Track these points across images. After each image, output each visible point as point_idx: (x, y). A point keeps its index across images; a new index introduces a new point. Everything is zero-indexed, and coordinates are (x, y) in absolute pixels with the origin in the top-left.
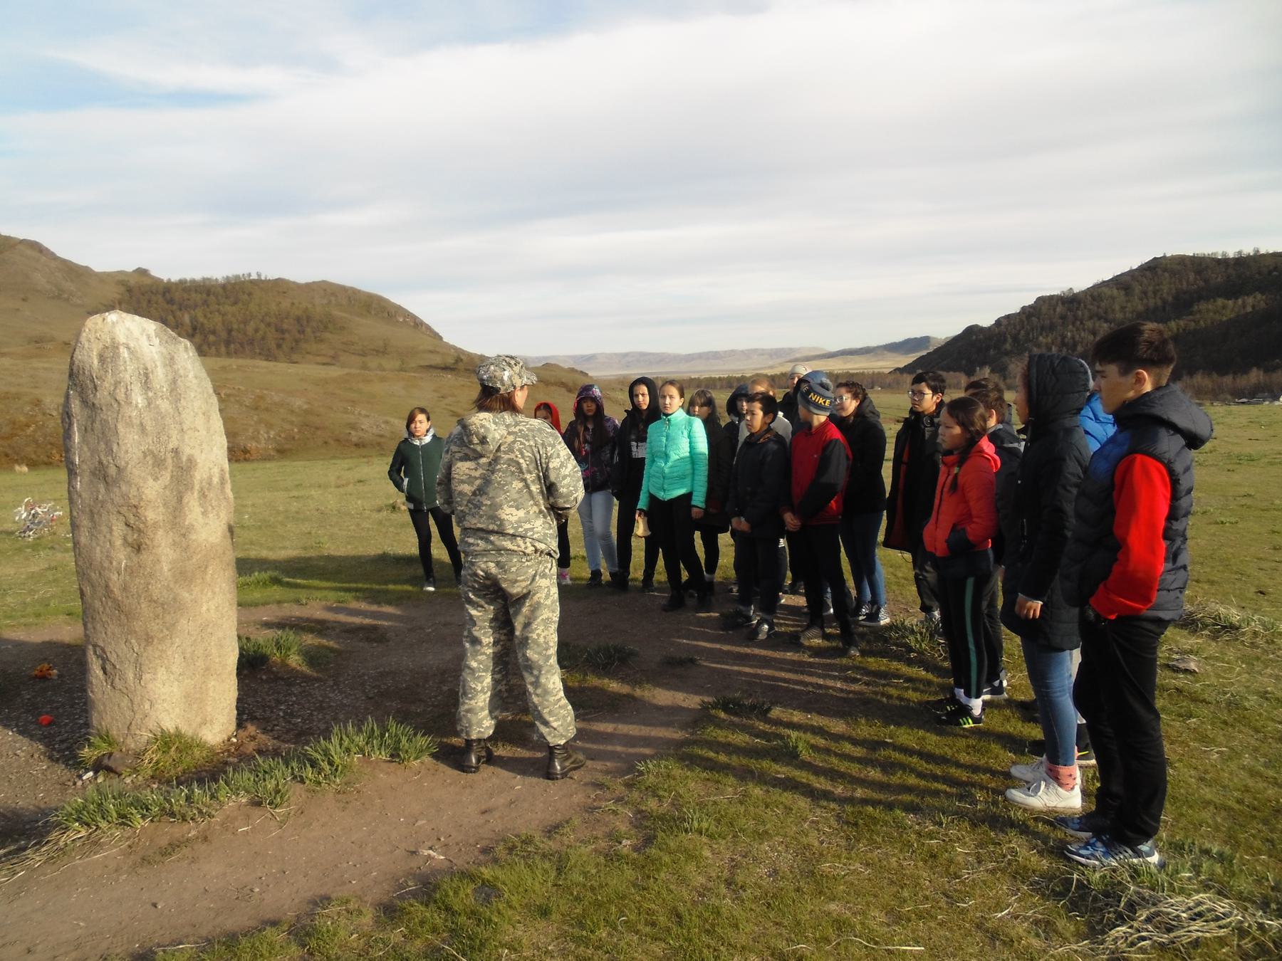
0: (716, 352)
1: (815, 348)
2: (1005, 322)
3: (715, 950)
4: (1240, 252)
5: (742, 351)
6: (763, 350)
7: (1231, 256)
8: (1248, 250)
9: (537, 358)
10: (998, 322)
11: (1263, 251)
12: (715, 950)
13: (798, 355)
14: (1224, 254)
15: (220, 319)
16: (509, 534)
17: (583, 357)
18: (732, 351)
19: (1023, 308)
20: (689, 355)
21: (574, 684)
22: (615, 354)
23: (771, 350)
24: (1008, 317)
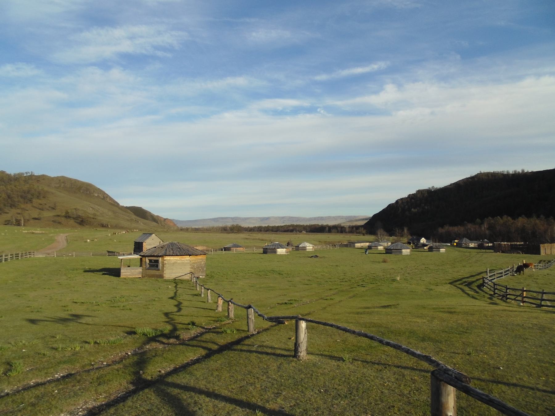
0: (322, 217)
1: (365, 216)
2: (400, 202)
3: (197, 379)
4: (515, 171)
5: (334, 217)
6: (342, 216)
7: (511, 172)
8: (519, 170)
9: (244, 218)
10: (397, 201)
11: (482, 172)
12: (197, 379)
13: (357, 218)
14: (508, 172)
15: (217, 389)
16: (295, 353)
17: (264, 218)
18: (329, 217)
19: (409, 195)
20: (310, 218)
21: (464, 404)
22: (279, 217)
23: (347, 216)
24: (402, 199)
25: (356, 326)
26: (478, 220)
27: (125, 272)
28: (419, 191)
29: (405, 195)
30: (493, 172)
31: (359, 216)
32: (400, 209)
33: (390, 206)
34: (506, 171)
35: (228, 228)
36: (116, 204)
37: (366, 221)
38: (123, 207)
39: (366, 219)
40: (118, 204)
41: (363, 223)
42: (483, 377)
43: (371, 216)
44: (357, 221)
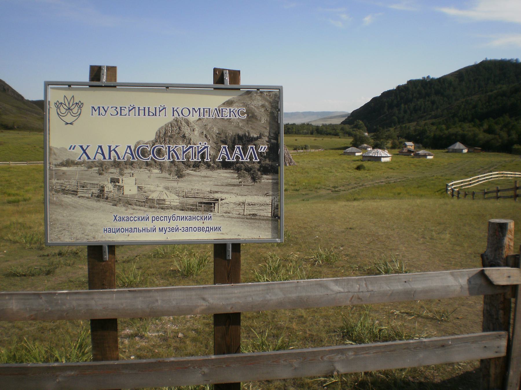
25: (439, 312)
26: (477, 121)
27: (383, 160)
28: (410, 82)
29: (392, 86)
30: (421, 78)
31: (332, 112)
32: (387, 104)
33: (375, 100)
34: (515, 58)
35: (70, 161)
36: (20, 98)
37: (343, 119)
38: (28, 101)
39: (342, 116)
40: (22, 98)
41: (338, 122)
42: (271, 286)
43: (350, 111)
44: (331, 118)
